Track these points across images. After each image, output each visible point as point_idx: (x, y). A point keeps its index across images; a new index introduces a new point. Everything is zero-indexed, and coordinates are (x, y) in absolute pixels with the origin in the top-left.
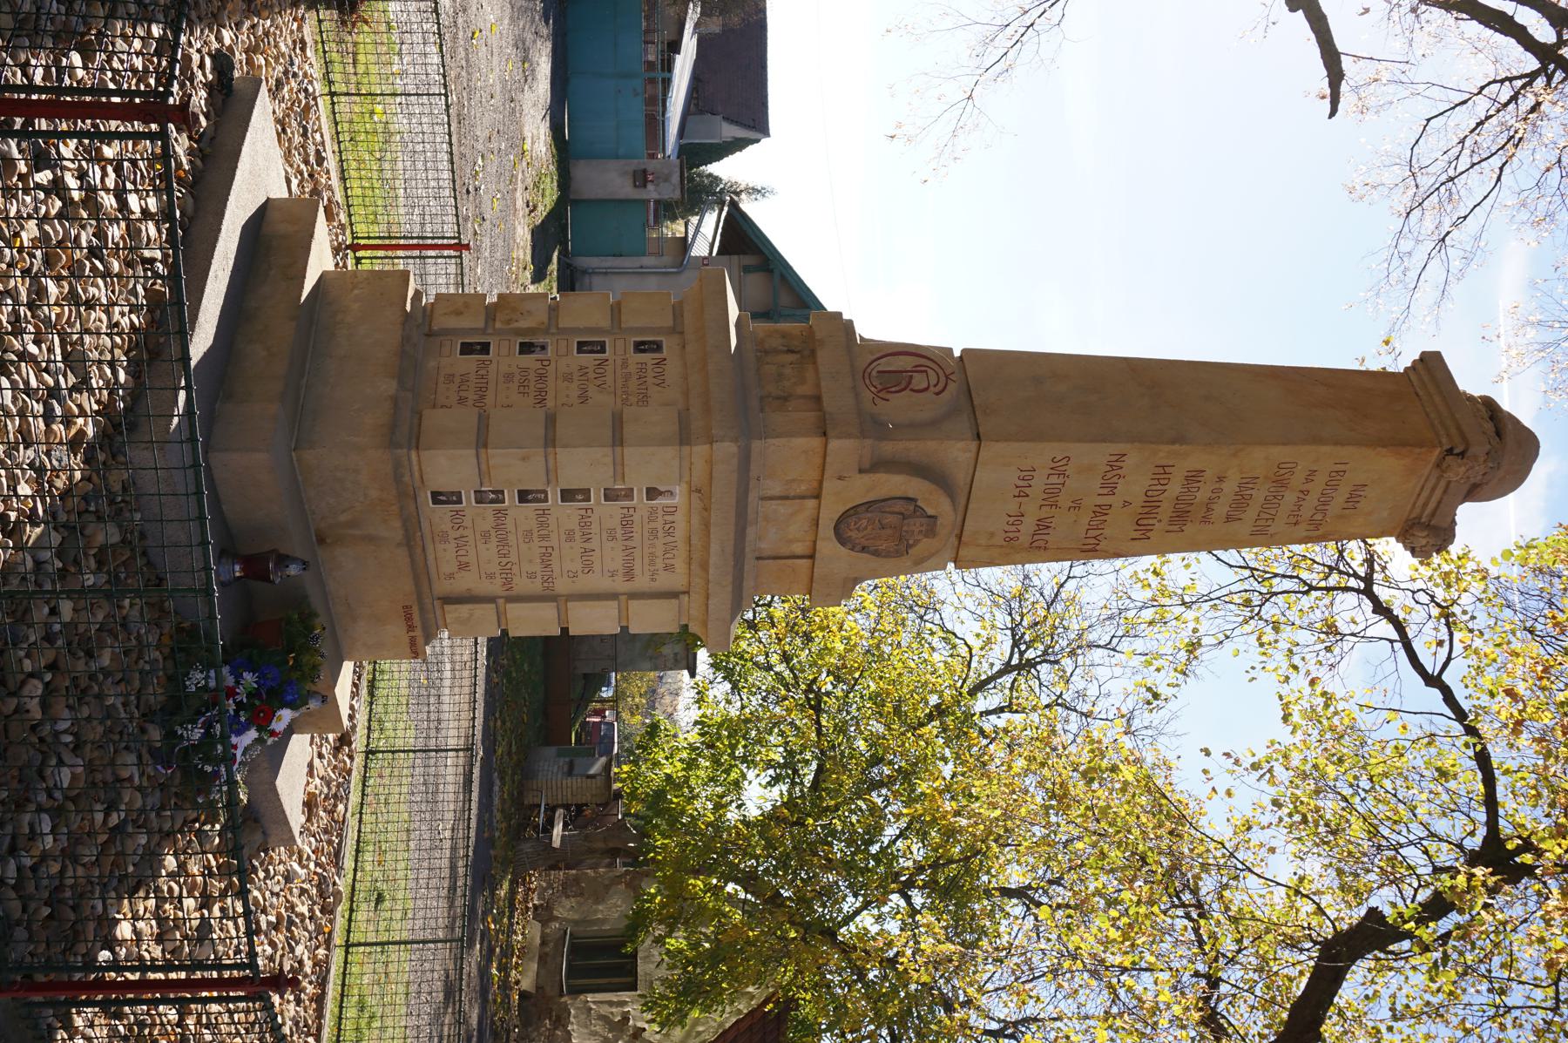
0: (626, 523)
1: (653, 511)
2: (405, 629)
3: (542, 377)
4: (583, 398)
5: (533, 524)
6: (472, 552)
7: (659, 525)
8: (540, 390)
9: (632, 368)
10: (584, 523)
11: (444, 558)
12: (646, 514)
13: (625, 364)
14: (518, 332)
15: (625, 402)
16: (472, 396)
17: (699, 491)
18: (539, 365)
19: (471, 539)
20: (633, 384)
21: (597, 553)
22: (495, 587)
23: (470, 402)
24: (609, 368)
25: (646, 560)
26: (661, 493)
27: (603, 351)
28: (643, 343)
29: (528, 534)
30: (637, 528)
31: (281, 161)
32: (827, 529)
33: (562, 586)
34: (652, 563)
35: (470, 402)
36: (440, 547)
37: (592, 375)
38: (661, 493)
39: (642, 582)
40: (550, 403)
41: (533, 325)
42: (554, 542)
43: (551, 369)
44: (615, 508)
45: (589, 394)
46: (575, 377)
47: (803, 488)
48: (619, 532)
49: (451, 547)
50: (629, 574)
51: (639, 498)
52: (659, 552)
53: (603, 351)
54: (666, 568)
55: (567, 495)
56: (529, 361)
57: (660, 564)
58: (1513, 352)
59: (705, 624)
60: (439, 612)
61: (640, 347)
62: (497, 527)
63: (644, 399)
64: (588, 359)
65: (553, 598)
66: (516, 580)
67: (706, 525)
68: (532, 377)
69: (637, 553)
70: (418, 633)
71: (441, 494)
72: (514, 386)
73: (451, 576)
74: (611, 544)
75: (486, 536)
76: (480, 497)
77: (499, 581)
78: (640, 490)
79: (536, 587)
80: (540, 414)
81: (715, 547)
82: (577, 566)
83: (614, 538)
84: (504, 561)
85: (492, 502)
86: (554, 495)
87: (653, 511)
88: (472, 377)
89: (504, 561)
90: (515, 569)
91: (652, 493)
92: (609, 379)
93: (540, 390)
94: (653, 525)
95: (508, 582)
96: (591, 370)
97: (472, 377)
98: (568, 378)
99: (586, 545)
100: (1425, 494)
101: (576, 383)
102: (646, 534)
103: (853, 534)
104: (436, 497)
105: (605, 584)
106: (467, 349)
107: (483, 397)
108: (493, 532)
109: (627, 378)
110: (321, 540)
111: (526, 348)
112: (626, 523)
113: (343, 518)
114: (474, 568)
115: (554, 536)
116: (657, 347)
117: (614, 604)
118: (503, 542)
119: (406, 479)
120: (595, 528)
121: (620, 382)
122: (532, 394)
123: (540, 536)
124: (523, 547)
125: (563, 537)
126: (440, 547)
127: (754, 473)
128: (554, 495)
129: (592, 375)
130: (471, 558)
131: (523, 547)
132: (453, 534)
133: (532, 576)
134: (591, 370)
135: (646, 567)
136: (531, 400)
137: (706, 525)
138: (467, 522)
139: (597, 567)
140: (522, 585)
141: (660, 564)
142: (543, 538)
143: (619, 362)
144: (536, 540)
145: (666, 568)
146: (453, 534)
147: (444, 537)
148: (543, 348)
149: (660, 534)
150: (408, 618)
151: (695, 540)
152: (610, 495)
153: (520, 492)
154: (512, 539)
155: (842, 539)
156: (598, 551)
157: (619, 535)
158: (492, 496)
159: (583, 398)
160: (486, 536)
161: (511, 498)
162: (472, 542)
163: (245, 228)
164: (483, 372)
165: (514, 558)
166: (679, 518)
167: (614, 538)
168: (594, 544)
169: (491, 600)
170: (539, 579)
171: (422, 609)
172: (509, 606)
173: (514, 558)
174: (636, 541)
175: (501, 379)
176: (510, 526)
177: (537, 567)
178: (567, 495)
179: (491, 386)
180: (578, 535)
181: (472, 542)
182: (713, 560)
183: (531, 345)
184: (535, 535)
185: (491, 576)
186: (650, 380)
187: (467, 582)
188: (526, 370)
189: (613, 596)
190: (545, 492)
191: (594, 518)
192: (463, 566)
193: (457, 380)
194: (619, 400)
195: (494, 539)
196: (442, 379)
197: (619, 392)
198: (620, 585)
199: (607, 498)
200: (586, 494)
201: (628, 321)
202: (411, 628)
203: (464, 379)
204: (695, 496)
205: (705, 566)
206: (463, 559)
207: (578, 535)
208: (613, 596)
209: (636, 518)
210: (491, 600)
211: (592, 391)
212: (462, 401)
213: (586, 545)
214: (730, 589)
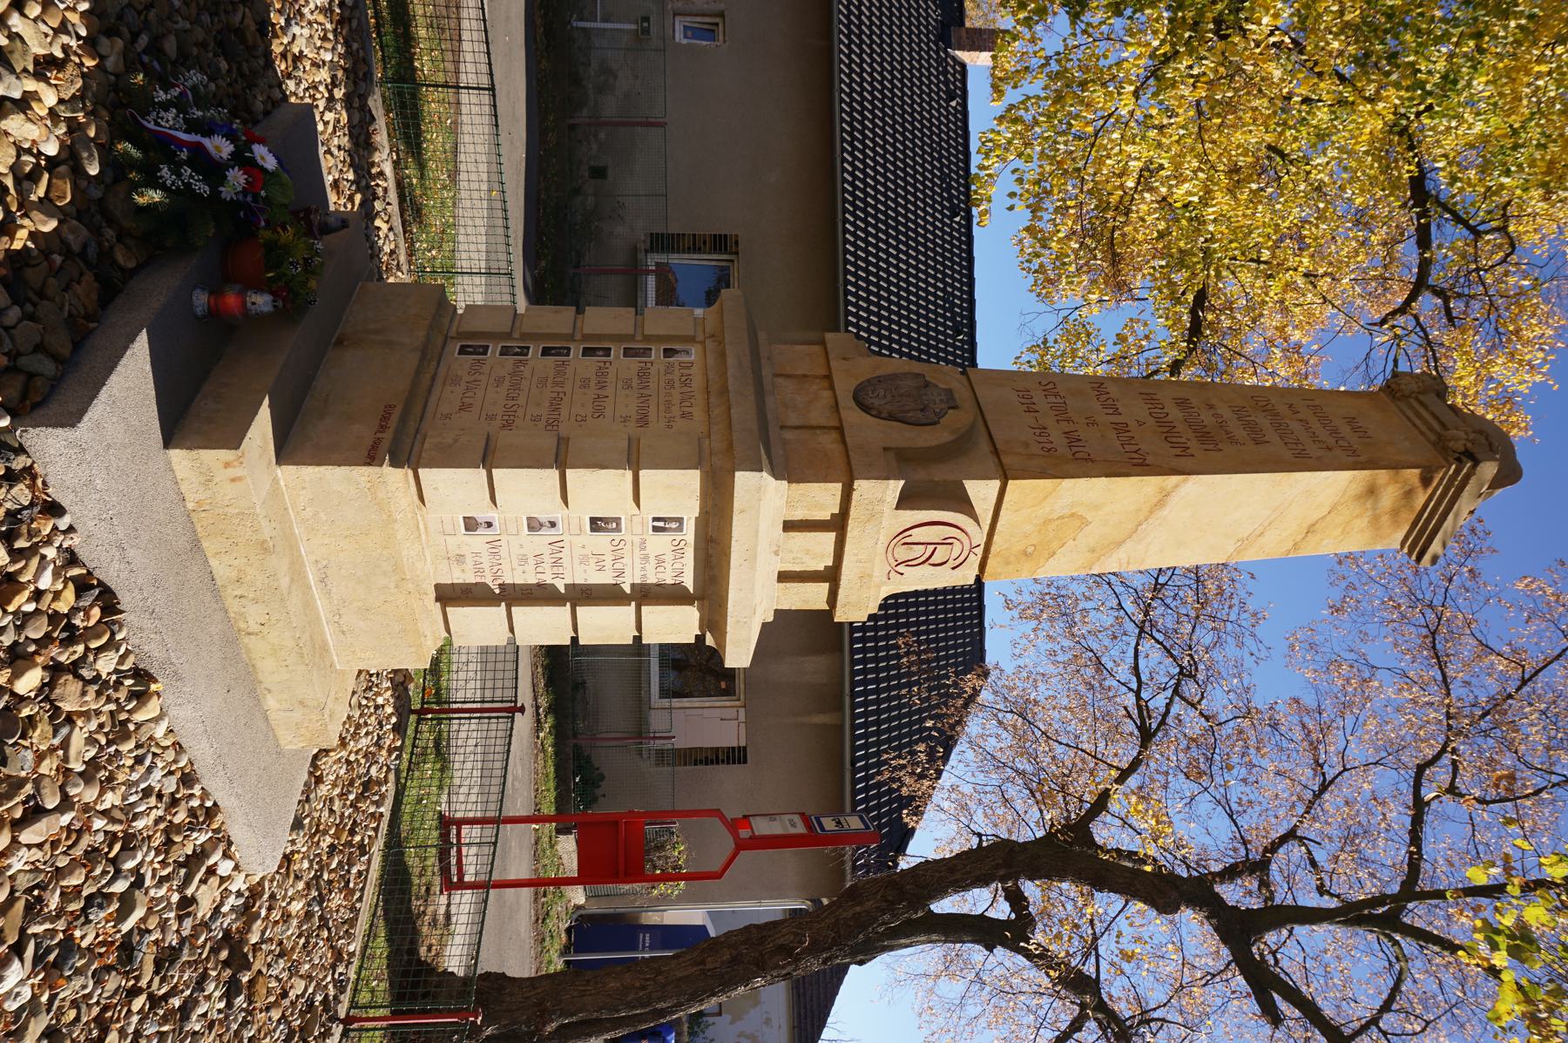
0: (643, 374)
1: (670, 366)
10: (601, 373)
25: (662, 407)
30: (653, 378)
32: (846, 401)
34: (668, 410)
42: (568, 388)
44: (634, 363)
47: (825, 515)
48: (635, 382)
51: (656, 353)
52: (676, 399)
57: (676, 411)
69: (653, 402)
70: (388, 436)
75: (499, 381)
81: (731, 361)
84: (511, 403)
89: (511, 403)
90: (520, 412)
100: (1418, 422)
102: (662, 384)
103: (876, 402)
108: (508, 378)
112: (643, 374)
120: (611, 378)
139: (608, 412)
141: (676, 411)
145: (683, 416)
146: (466, 378)
149: (677, 384)
155: (865, 408)
157: (635, 385)
165: (522, 401)
168: (609, 391)
171: (403, 420)
182: (732, 384)
184: (550, 381)
202: (382, 428)
209: (653, 370)
214: (752, 398)
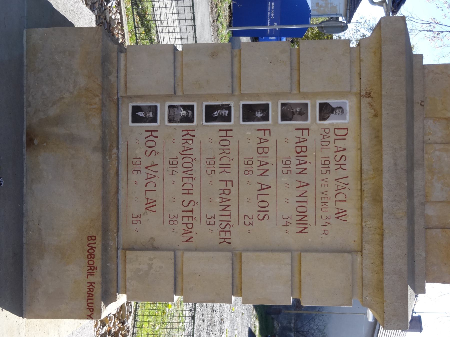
0: (301, 150)
1: (325, 132)
7: (330, 153)
12: (319, 138)
17: (368, 95)
25: (319, 204)
31: (93, 326)
39: (314, 235)
49: (141, 178)
67: (378, 138)
74: (285, 179)
78: (314, 106)
81: (387, 158)
83: (289, 171)
84: (188, 198)
87: (325, 132)
89: (188, 198)
91: (326, 110)
110: (30, 141)
112: (301, 150)
113: (53, 112)
114: (158, 207)
115: (234, 165)
117: (289, 254)
119: (113, 78)
120: (271, 158)
137: (378, 138)
144: (218, 170)
146: (146, 161)
158: (183, 112)
161: (199, 114)
163: (51, 4)
165: (196, 197)
166: (350, 143)
171: (105, 248)
173: (196, 197)
176: (195, 153)
177: (216, 210)
195: (180, 169)
198: (292, 238)
204: (365, 101)
205: (377, 199)
206: (150, 195)
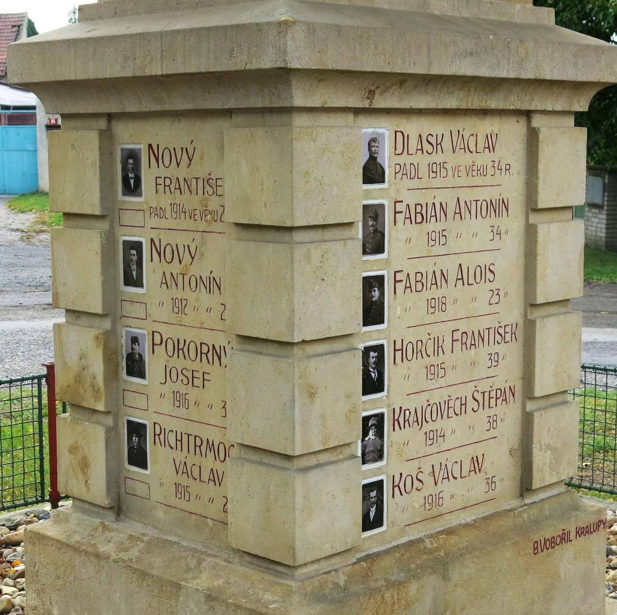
0: (418, 215)
1: (401, 171)
2: (565, 545)
3: (179, 348)
4: (213, 284)
5: (418, 365)
6: (456, 455)
7: (423, 161)
8: (199, 353)
9: (165, 201)
11: (464, 498)
13: (158, 212)
14: (111, 375)
15: (217, 217)
16: (209, 463)
18: (160, 350)
19: (435, 460)
20: (190, 201)
21: (464, 260)
22: (509, 416)
23: (218, 466)
24: (166, 238)
25: (478, 181)
26: (372, 159)
27: (138, 246)
28: (126, 180)
29: (432, 371)
30: (426, 198)
33: (511, 313)
34: (482, 172)
35: (218, 466)
36: (448, 504)
37: (175, 268)
38: (372, 159)
39: (511, 187)
40: (220, 340)
41: (100, 352)
42: (443, 331)
43: (167, 332)
44: (396, 234)
45: (205, 275)
46: (180, 294)
48: (432, 226)
49: (446, 487)
50: (498, 207)
53: (138, 246)
54: (491, 148)
55: (373, 313)
56: (154, 364)
57: (484, 159)
58: (324, 29)
59: (577, 86)
60: (542, 495)
61: (132, 187)
62: (420, 421)
63: (212, 184)
64: (151, 270)
65: (530, 327)
66: (499, 383)
68: (179, 363)
69: (466, 196)
71: (366, 516)
72: (193, 394)
73: (490, 482)
76: (373, 454)
77: (500, 409)
78: (367, 194)
79: (511, 352)
80: (237, 359)
82: (482, 290)
83: (443, 234)
84: (471, 404)
85: (380, 434)
86: (374, 335)
88: (180, 456)
89: (471, 404)
90: (484, 386)
91: (373, 173)
92: (181, 239)
93: (199, 353)
94: (423, 171)
95: (503, 395)
96: (168, 269)
97: (180, 456)
98: (180, 306)
99: (452, 278)
101: (188, 294)
102: (437, 182)
104: (371, 522)
105: (512, 245)
106: (138, 458)
107: (211, 446)
108: (427, 427)
109: (179, 210)
111: (136, 367)
112: (418, 215)
114: (478, 450)
115: (436, 331)
116: (132, 157)
118: (442, 410)
120: (426, 266)
121: (186, 223)
122: (206, 367)
123: (436, 353)
124: (451, 378)
125: (439, 316)
126: (448, 504)
127: (324, 357)
128: (374, 335)
129: (175, 268)
130: (464, 456)
131: (451, 378)
132: (429, 488)
133: (495, 359)
134: (168, 269)
135: (488, 180)
136: (215, 370)
138: (410, 469)
139: (484, 260)
140: (508, 374)
142: (439, 348)
143: (154, 222)
144: (442, 358)
145: (491, 148)
147: (434, 500)
148: (135, 340)
149: (438, 158)
150: (551, 543)
151: (451, 103)
152: (374, 243)
153: (366, 392)
154: (437, 397)
156: (462, 259)
157: (439, 226)
158: (371, 435)
159: (213, 284)
160: (432, 437)
162: (442, 458)
164: (172, 439)
167: (443, 234)
169: (527, 421)
170: (502, 349)
172: (538, 392)
174: (448, 198)
175: (182, 412)
176: (418, 402)
177: (483, 352)
178: (373, 313)
179: (194, 429)
180: (436, 293)
181: (442, 458)
183: (130, 357)
184: (433, 360)
185: (493, 422)
186: (182, 173)
187: (500, 461)
188: (168, 372)
189: (531, 233)
190: (367, 350)
191: (409, 268)
192: (477, 464)
193: (183, 480)
194: (218, 227)
195: (439, 424)
196: (183, 504)
197: (202, 226)
198: (513, 223)
199: (379, 248)
200: (373, 284)
201: (92, 205)
202: (565, 538)
203: (182, 469)
206: (466, 467)
207: (436, 293)
208: (531, 233)
209: (411, 199)
210: (527, 421)
211: (200, 269)
212: (216, 479)
213: (452, 278)
